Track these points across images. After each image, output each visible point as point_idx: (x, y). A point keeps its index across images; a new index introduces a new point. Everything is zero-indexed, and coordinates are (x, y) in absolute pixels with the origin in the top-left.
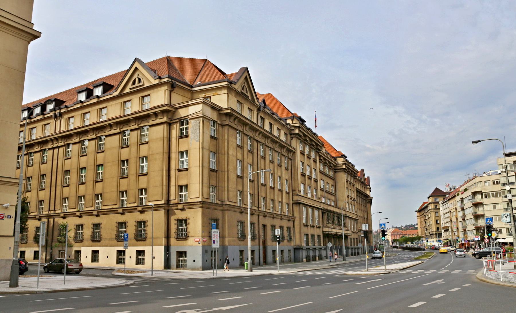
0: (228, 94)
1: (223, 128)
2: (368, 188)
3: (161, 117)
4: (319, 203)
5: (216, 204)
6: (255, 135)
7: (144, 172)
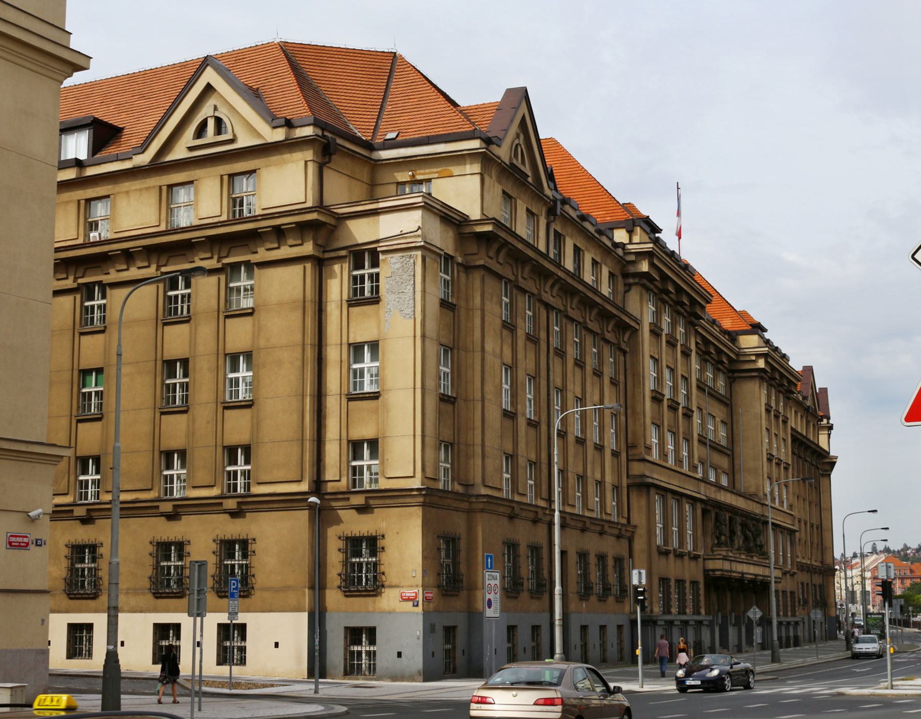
0: (481, 174)
1: (470, 276)
2: (823, 428)
3: (294, 240)
4: (696, 481)
5: (452, 492)
6: (542, 289)
7: (241, 398)
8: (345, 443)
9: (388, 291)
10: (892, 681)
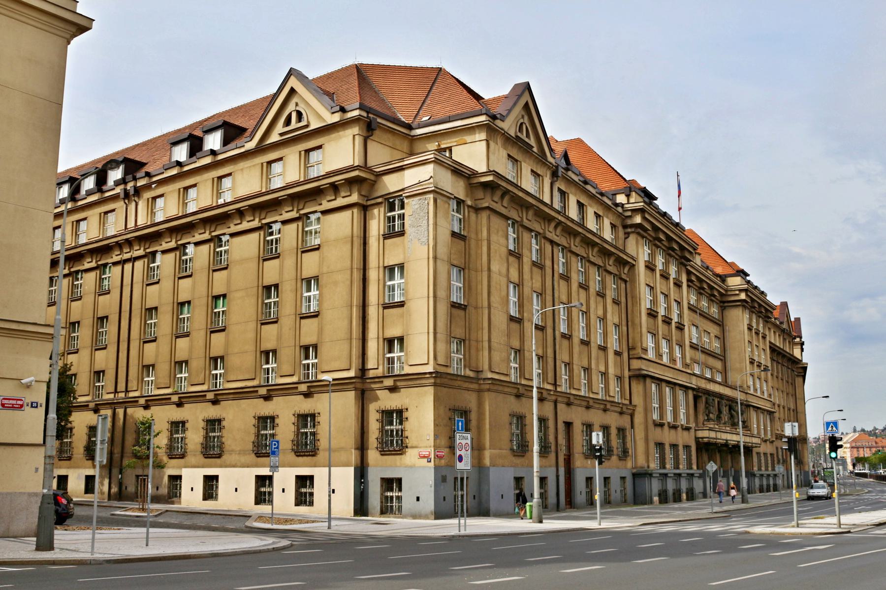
0: (487, 140)
1: (479, 215)
2: (797, 344)
4: (688, 375)
5: (464, 376)
8: (381, 340)
9: (412, 226)
10: (798, 520)
